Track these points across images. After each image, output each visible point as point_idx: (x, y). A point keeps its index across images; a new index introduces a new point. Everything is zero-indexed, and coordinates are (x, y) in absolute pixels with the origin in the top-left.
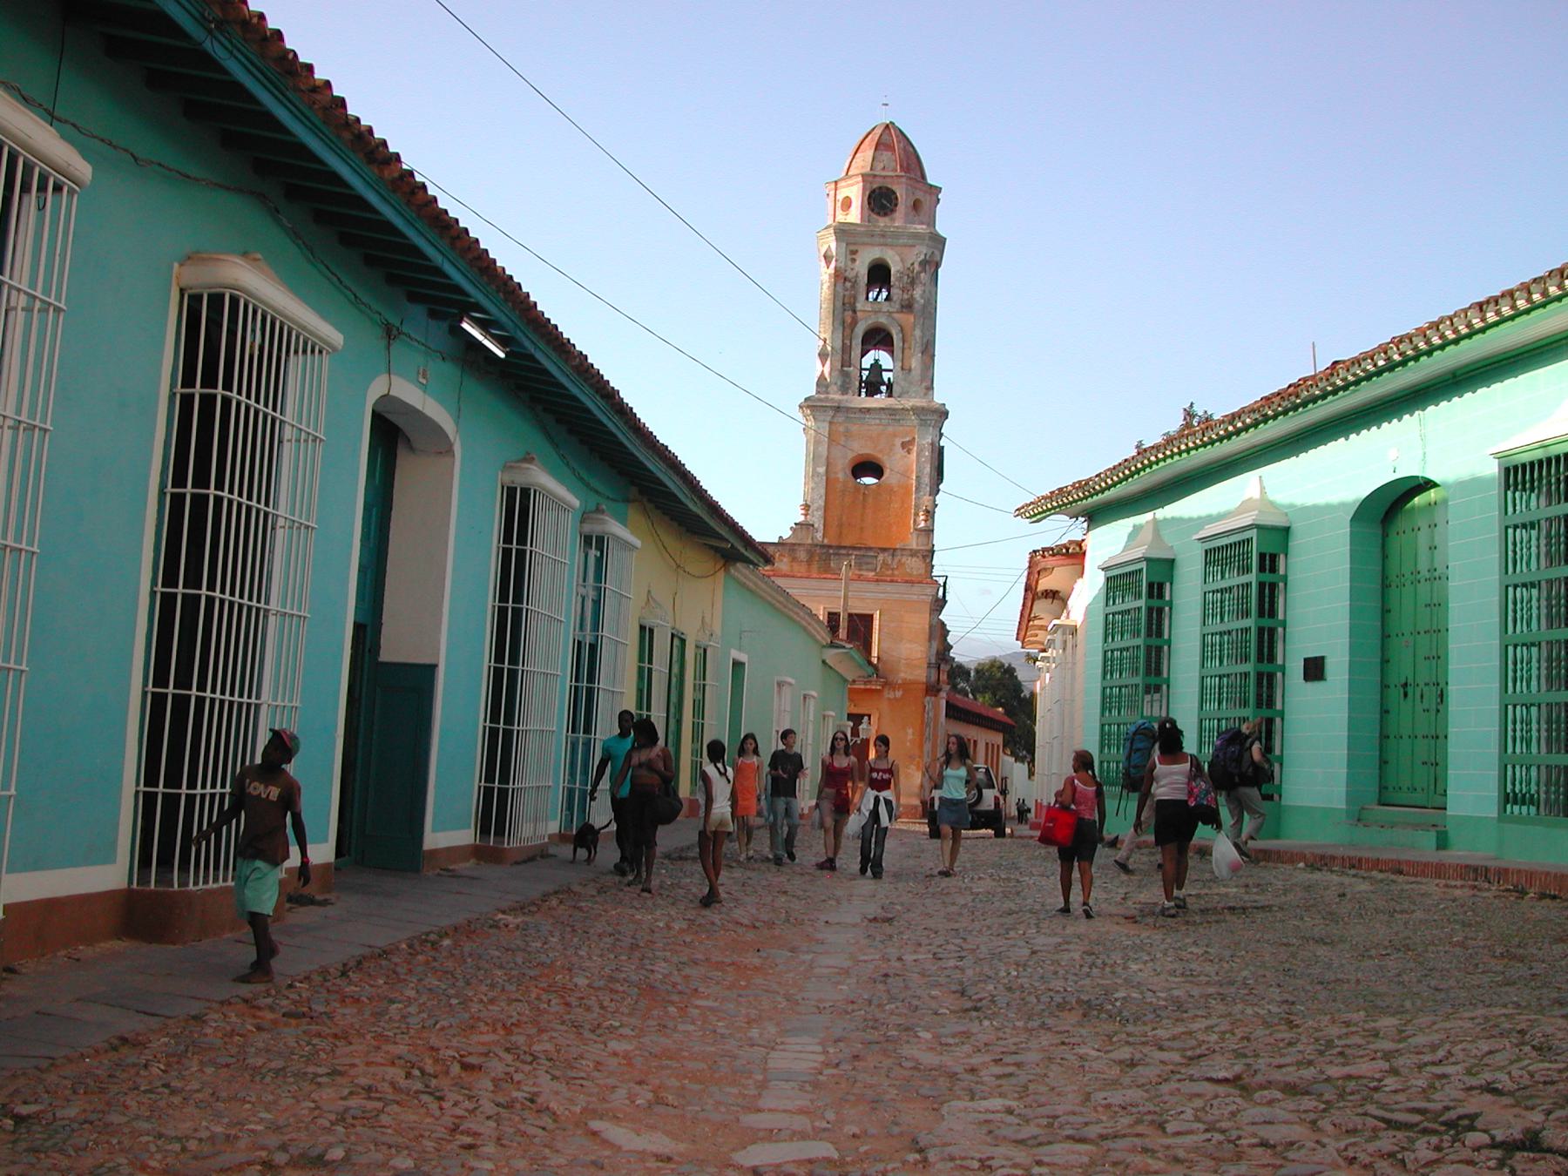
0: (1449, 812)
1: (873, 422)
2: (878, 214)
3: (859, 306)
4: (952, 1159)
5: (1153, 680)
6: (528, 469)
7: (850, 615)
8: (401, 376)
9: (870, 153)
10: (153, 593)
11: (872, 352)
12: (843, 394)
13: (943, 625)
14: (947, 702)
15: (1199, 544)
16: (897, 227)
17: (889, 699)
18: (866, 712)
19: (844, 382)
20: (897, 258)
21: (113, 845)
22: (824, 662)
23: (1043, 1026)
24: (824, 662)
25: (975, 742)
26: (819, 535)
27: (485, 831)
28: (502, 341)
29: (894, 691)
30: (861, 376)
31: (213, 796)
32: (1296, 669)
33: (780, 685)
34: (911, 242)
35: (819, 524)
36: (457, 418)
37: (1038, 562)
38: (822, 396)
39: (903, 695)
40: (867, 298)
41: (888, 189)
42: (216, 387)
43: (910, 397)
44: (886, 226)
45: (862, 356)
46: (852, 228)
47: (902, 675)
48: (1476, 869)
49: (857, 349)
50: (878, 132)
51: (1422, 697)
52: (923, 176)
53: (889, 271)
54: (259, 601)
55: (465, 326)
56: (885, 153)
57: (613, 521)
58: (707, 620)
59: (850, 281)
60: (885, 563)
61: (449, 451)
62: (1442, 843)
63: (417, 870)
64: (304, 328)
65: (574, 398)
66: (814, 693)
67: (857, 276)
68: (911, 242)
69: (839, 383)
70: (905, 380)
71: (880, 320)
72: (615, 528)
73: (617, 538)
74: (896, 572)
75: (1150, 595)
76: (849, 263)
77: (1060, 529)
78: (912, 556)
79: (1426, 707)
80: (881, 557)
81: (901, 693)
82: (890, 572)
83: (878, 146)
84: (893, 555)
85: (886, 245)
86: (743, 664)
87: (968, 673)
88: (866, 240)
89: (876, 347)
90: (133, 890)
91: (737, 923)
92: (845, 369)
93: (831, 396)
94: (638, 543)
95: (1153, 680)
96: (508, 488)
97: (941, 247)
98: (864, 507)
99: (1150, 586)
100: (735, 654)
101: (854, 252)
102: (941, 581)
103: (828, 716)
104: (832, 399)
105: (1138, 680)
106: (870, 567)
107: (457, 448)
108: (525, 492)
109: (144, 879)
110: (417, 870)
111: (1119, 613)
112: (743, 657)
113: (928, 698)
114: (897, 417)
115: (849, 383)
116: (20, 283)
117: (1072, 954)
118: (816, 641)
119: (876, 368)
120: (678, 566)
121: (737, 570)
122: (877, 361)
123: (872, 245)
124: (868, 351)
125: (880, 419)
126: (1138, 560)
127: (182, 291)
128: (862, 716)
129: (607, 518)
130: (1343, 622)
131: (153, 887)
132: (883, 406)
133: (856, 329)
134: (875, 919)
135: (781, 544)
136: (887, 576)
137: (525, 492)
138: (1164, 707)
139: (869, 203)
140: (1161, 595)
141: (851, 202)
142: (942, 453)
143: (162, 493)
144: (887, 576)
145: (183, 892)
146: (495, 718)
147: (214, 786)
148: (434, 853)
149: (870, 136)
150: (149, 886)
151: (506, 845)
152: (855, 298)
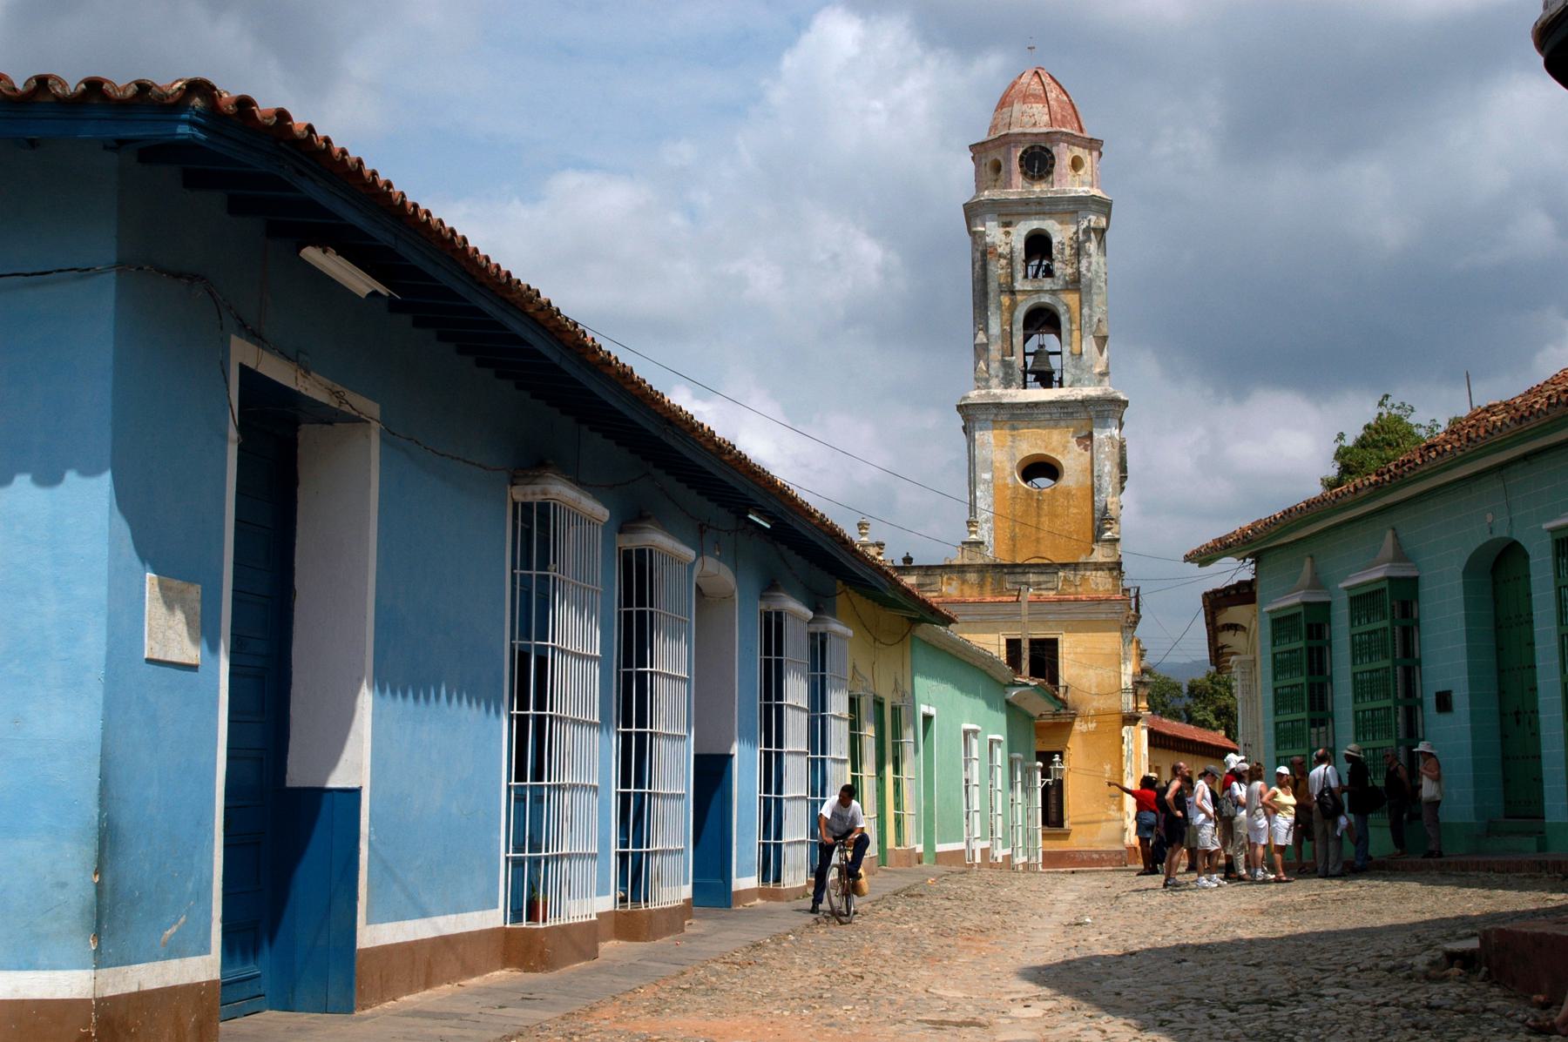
0: (1547, 821)
1: (1043, 417)
3: (1018, 286)
5: (1318, 715)
12: (1006, 388)
15: (1346, 592)
17: (1082, 733)
18: (1059, 749)
19: (1006, 373)
21: (497, 902)
27: (765, 879)
28: (767, 518)
29: (1086, 722)
30: (1025, 364)
32: (1430, 701)
38: (983, 392)
39: (1096, 728)
43: (1084, 385)
44: (1042, 191)
47: (1095, 704)
48: (1540, 864)
53: (1050, 242)
55: (751, 516)
58: (900, 682)
59: (1005, 258)
60: (1066, 579)
62: (1542, 848)
67: (1012, 252)
69: (1001, 375)
71: (1042, 300)
74: (1080, 589)
75: (1310, 637)
77: (1231, 571)
78: (1096, 570)
81: (1094, 725)
82: (1072, 590)
89: (1037, 331)
92: (1007, 358)
95: (1318, 715)
96: (765, 613)
98: (1039, 515)
99: (1309, 627)
100: (924, 709)
104: (994, 395)
105: (1304, 715)
110: (730, 907)
112: (932, 711)
113: (1126, 728)
115: (1012, 375)
120: (875, 639)
124: (1031, 336)
125: (1050, 414)
126: (1297, 605)
130: (1462, 661)
133: (1016, 313)
134: (1070, 924)
136: (1070, 594)
137: (779, 614)
138: (1331, 739)
140: (1320, 636)
141: (1000, 166)
144: (1070, 594)
145: (635, 912)
146: (767, 789)
148: (738, 892)
152: (1012, 276)
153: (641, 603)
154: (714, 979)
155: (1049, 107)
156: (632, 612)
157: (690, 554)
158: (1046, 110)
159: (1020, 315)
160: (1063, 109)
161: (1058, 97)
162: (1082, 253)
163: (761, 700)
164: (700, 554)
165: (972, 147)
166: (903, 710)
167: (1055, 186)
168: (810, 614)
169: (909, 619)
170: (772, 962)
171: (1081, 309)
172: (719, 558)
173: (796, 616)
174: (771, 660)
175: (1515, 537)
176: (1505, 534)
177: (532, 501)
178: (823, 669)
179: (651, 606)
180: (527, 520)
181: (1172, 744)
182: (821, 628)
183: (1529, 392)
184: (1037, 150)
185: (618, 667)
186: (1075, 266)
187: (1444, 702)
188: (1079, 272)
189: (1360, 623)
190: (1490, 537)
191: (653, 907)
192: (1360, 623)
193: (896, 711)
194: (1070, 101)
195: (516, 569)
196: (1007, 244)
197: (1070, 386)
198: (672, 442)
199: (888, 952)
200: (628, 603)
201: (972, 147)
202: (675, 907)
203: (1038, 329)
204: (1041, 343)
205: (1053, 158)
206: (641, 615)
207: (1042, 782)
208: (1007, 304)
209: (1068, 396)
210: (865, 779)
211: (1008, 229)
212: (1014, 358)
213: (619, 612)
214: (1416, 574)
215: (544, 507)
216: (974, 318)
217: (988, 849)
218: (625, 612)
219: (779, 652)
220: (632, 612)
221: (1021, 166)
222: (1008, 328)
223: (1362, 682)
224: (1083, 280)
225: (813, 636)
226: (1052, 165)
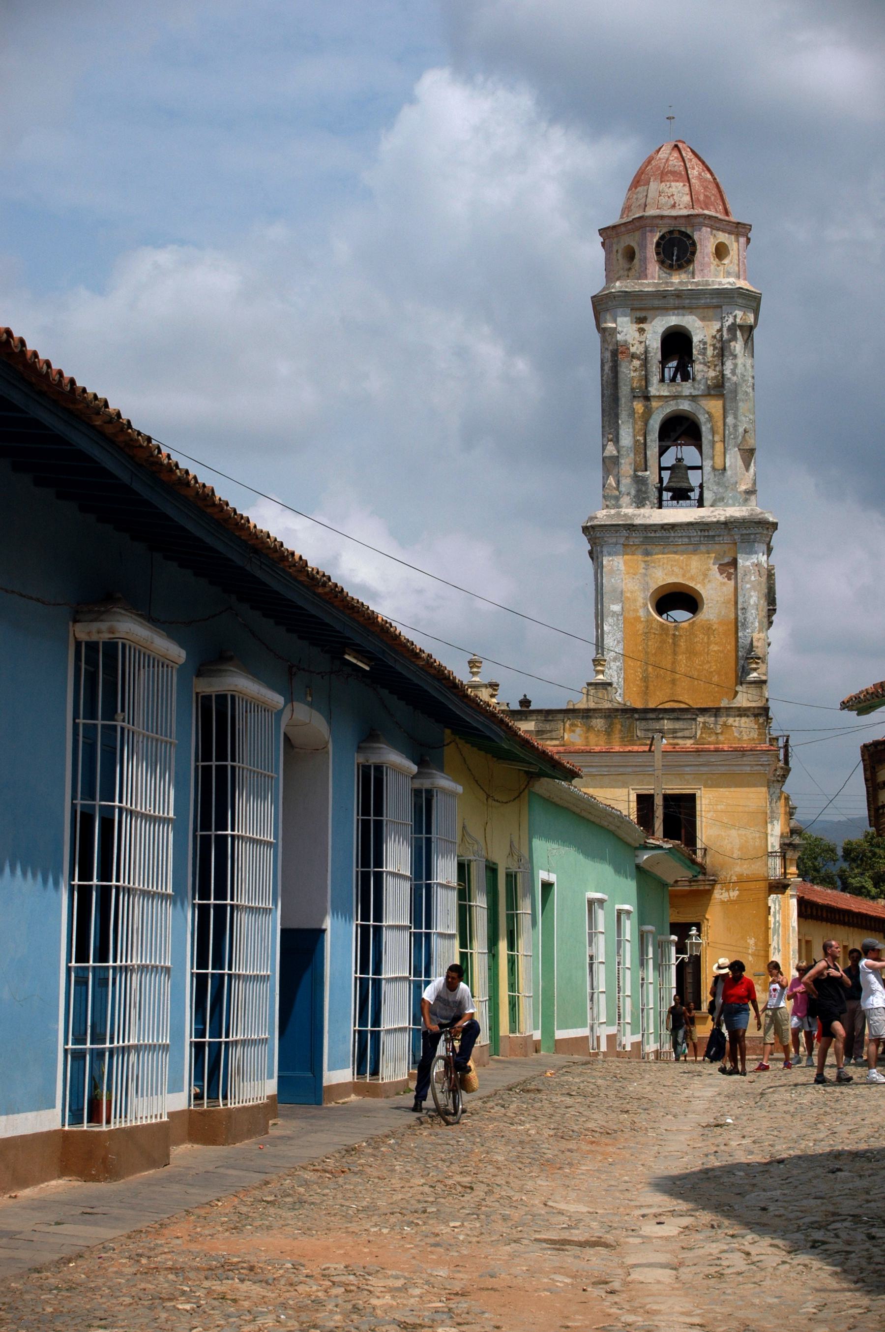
1: (680, 541)
3: (653, 391)
4: (747, 1207)
6: (381, 748)
8: (297, 701)
11: (673, 449)
16: (697, 284)
17: (723, 902)
18: (695, 920)
19: (639, 491)
29: (728, 890)
30: (661, 480)
34: (715, 301)
38: (613, 512)
43: (727, 505)
44: (681, 283)
47: (738, 869)
57: (438, 773)
58: (516, 844)
63: (319, 1102)
65: (426, 691)
66: (627, 907)
68: (715, 301)
69: (633, 492)
70: (718, 484)
73: (444, 791)
78: (740, 716)
80: (700, 719)
81: (737, 893)
82: (713, 738)
87: (833, 851)
88: (656, 303)
90: (191, 1110)
91: (593, 1131)
92: (640, 474)
93: (624, 511)
96: (362, 766)
100: (543, 875)
104: (625, 515)
106: (687, 733)
108: (379, 769)
109: (63, 1125)
110: (319, 1102)
112: (553, 878)
113: (773, 896)
114: (711, 533)
116: (171, 737)
120: (488, 796)
124: (668, 448)
125: (689, 537)
128: (688, 926)
129: (434, 771)
131: (205, 1107)
132: (692, 520)
133: (651, 422)
134: (708, 1126)
137: (379, 769)
143: (195, 837)
150: (203, 1107)
153: (222, 756)
154: (302, 1190)
157: (277, 700)
158: (687, 189)
159: (655, 423)
161: (700, 174)
162: (726, 353)
167: (696, 277)
168: (414, 768)
171: (725, 418)
172: (311, 705)
173: (398, 770)
178: (429, 831)
179: (233, 760)
182: (426, 784)
184: (676, 235)
185: (195, 830)
186: (718, 368)
188: (723, 376)
191: (233, 1106)
193: (511, 878)
194: (715, 179)
196: (641, 342)
197: (712, 506)
200: (207, 757)
201: (602, 232)
203: (676, 440)
204: (679, 457)
205: (694, 244)
206: (222, 770)
207: (677, 958)
208: (641, 411)
209: (709, 517)
211: (642, 325)
212: (648, 473)
213: (197, 767)
215: (111, 648)
216: (603, 427)
218: (202, 766)
219: (379, 811)
221: (658, 254)
222: (641, 439)
224: (727, 384)
225: (417, 793)
226: (693, 253)
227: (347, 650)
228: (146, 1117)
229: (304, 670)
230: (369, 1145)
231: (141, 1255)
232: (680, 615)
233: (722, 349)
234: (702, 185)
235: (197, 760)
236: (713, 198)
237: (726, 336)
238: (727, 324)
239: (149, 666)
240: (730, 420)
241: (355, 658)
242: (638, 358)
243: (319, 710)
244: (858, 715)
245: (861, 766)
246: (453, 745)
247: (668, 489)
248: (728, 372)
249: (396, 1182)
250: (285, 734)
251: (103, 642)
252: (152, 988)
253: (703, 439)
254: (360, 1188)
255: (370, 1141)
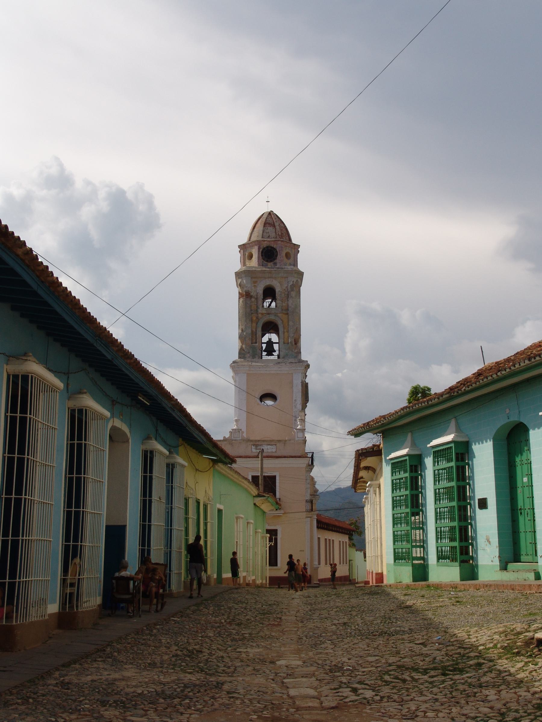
0: (539, 564)
2: (267, 261)
5: (415, 510)
7: (265, 477)
9: (262, 228)
10: (64, 511)
13: (312, 478)
14: (317, 520)
20: (278, 284)
22: (255, 504)
23: (367, 638)
24: (255, 504)
25: (333, 540)
26: (245, 435)
31: (26, 581)
33: (237, 518)
35: (244, 429)
36: (130, 427)
37: (361, 455)
40: (263, 306)
41: (272, 247)
42: (17, 413)
45: (262, 337)
46: (254, 269)
49: (259, 333)
50: (265, 216)
51: (527, 514)
52: (290, 239)
54: (31, 497)
56: (269, 228)
61: (128, 441)
64: (96, 411)
66: (252, 521)
72: (180, 460)
75: (411, 471)
76: (253, 288)
79: (530, 519)
83: (266, 224)
84: (285, 444)
85: (272, 278)
86: (222, 510)
92: (254, 344)
94: (186, 464)
95: (415, 510)
97: (301, 277)
101: (255, 282)
102: (310, 455)
103: (258, 532)
105: (408, 510)
107: (130, 441)
111: (398, 479)
112: (221, 507)
117: (378, 621)
118: (251, 494)
119: (270, 343)
121: (219, 466)
122: (270, 339)
123: (265, 278)
127: (68, 408)
135: (225, 440)
137: (152, 452)
139: (262, 256)
142: (307, 387)
143: (66, 477)
147: (26, 578)
149: (261, 219)
151: (19, 623)
153: (80, 438)
154: (116, 654)
155: (275, 229)
156: (74, 443)
157: (107, 414)
158: (274, 230)
160: (281, 230)
161: (279, 224)
162: (289, 296)
163: (141, 497)
164: (113, 416)
165: (239, 246)
166: (209, 505)
168: (167, 453)
169: (212, 460)
170: (149, 642)
172: (122, 420)
173: (161, 453)
174: (147, 476)
175: (522, 420)
176: (516, 419)
177: (18, 373)
178: (172, 483)
179: (85, 440)
180: (15, 384)
181: (325, 527)
182: (171, 461)
183: (517, 354)
185: (66, 474)
186: (286, 302)
187: (483, 504)
188: (288, 305)
189: (395, 475)
190: (508, 421)
191: (81, 610)
192: (395, 475)
193: (205, 506)
195: (8, 413)
197: (283, 358)
198: (100, 348)
199: (211, 634)
200: (72, 438)
201: (239, 246)
202: (92, 610)
203: (269, 331)
206: (79, 445)
210: (190, 539)
211: (255, 284)
212: (257, 344)
213: (67, 444)
214: (467, 440)
215: (25, 378)
216: (239, 325)
217: (246, 576)
218: (70, 443)
219: (151, 472)
220: (74, 443)
223: (396, 501)
224: (290, 309)
225: (168, 465)
226: (277, 256)
227: (140, 394)
228: (37, 617)
229: (119, 403)
230: (147, 628)
231: (30, 698)
232: (269, 402)
233: (288, 295)
234: (280, 229)
235: (67, 440)
236: (284, 234)
237: (289, 289)
238: (290, 285)
239: (44, 391)
240: (291, 323)
241: (143, 398)
242: (254, 298)
243: (125, 423)
244: (355, 437)
245: (354, 459)
246: (182, 446)
247: (265, 351)
248: (290, 304)
249: (163, 649)
250: (109, 435)
251: (22, 375)
252: (26, 597)
253: (280, 331)
254: (146, 652)
255: (147, 627)
